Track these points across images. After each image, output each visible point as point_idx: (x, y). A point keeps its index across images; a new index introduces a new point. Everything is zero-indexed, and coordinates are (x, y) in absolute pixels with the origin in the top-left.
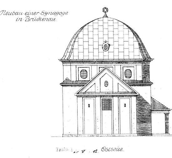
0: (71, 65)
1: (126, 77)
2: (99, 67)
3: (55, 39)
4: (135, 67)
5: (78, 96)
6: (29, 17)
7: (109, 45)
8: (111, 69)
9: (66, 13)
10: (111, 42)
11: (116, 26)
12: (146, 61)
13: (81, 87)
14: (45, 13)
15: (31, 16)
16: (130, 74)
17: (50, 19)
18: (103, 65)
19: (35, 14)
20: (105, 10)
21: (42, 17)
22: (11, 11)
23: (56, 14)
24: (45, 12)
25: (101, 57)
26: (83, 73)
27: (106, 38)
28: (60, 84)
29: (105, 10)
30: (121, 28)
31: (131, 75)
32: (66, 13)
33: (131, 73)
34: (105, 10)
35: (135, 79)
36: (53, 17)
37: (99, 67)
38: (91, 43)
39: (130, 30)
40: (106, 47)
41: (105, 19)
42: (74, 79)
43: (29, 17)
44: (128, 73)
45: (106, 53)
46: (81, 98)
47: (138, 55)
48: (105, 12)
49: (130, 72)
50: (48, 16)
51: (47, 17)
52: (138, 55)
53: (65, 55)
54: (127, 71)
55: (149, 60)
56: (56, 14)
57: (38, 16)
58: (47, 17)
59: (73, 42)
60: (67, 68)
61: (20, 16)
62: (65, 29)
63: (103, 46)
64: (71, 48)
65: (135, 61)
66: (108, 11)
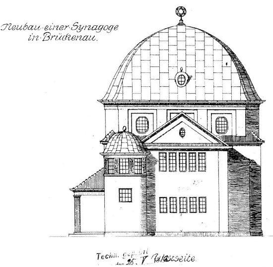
2: (128, 110)
3: (93, 68)
7: (189, 78)
8: (191, 116)
9: (116, 28)
12: (252, 104)
13: (160, 141)
14: (78, 28)
15: (54, 32)
16: (147, 125)
17: (86, 38)
18: (179, 109)
19: (58, 28)
20: (181, 12)
21: (73, 33)
22: (22, 23)
23: (97, 28)
24: (78, 25)
27: (182, 64)
28: (101, 141)
29: (181, 12)
32: (116, 28)
33: (148, 124)
34: (181, 12)
35: (234, 134)
36: (92, 33)
37: (128, 110)
38: (155, 71)
39: (225, 52)
40: (184, 80)
41: (181, 28)
44: (222, 123)
45: (182, 90)
47: (238, 95)
48: (181, 16)
49: (146, 122)
50: (84, 33)
51: (82, 33)
52: (238, 95)
55: (257, 102)
56: (97, 28)
57: (64, 33)
58: (82, 33)
60: (112, 112)
61: (36, 33)
62: (109, 50)
64: (118, 81)
65: (237, 104)
66: (185, 14)
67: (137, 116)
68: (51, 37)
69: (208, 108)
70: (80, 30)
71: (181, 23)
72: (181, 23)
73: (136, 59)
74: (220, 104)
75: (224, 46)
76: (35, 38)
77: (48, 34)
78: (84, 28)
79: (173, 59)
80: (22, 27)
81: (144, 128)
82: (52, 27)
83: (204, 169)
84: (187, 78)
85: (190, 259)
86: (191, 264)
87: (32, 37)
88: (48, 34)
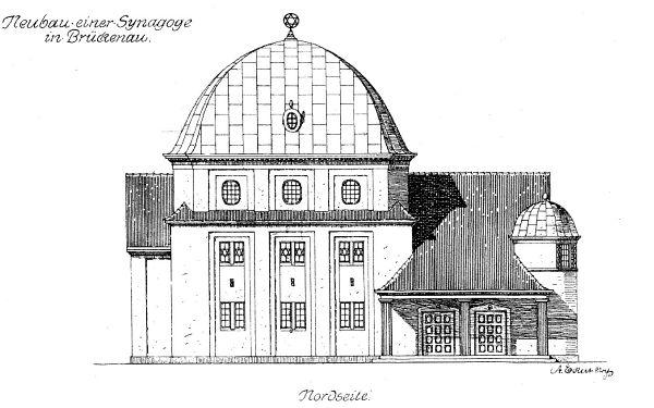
0: (195, 167)
1: (285, 201)
4: (370, 178)
5: (132, 254)
6: (94, 32)
10: (305, 106)
11: (319, 62)
19: (96, 23)
20: (291, 21)
22: (36, 16)
24: (127, 19)
25: (278, 150)
26: (348, 196)
27: (292, 94)
29: (291, 21)
30: (334, 68)
31: (239, 195)
33: (359, 190)
40: (294, 121)
42: (201, 207)
43: (94, 32)
45: (292, 137)
46: (143, 259)
53: (180, 143)
54: (357, 187)
59: (201, 105)
61: (56, 31)
63: (285, 118)
67: (223, 179)
68: (79, 37)
69: (212, 167)
70: (131, 25)
71: (291, 36)
72: (291, 36)
73: (222, 88)
74: (346, 160)
75: (370, 90)
76: (55, 40)
77: (76, 33)
78: (137, 23)
79: (278, 85)
80: (38, 23)
81: (348, 188)
82: (89, 22)
83: (242, 324)
84: (299, 118)
85: (360, 396)
86: (360, 404)
87: (50, 37)
88: (76, 33)
